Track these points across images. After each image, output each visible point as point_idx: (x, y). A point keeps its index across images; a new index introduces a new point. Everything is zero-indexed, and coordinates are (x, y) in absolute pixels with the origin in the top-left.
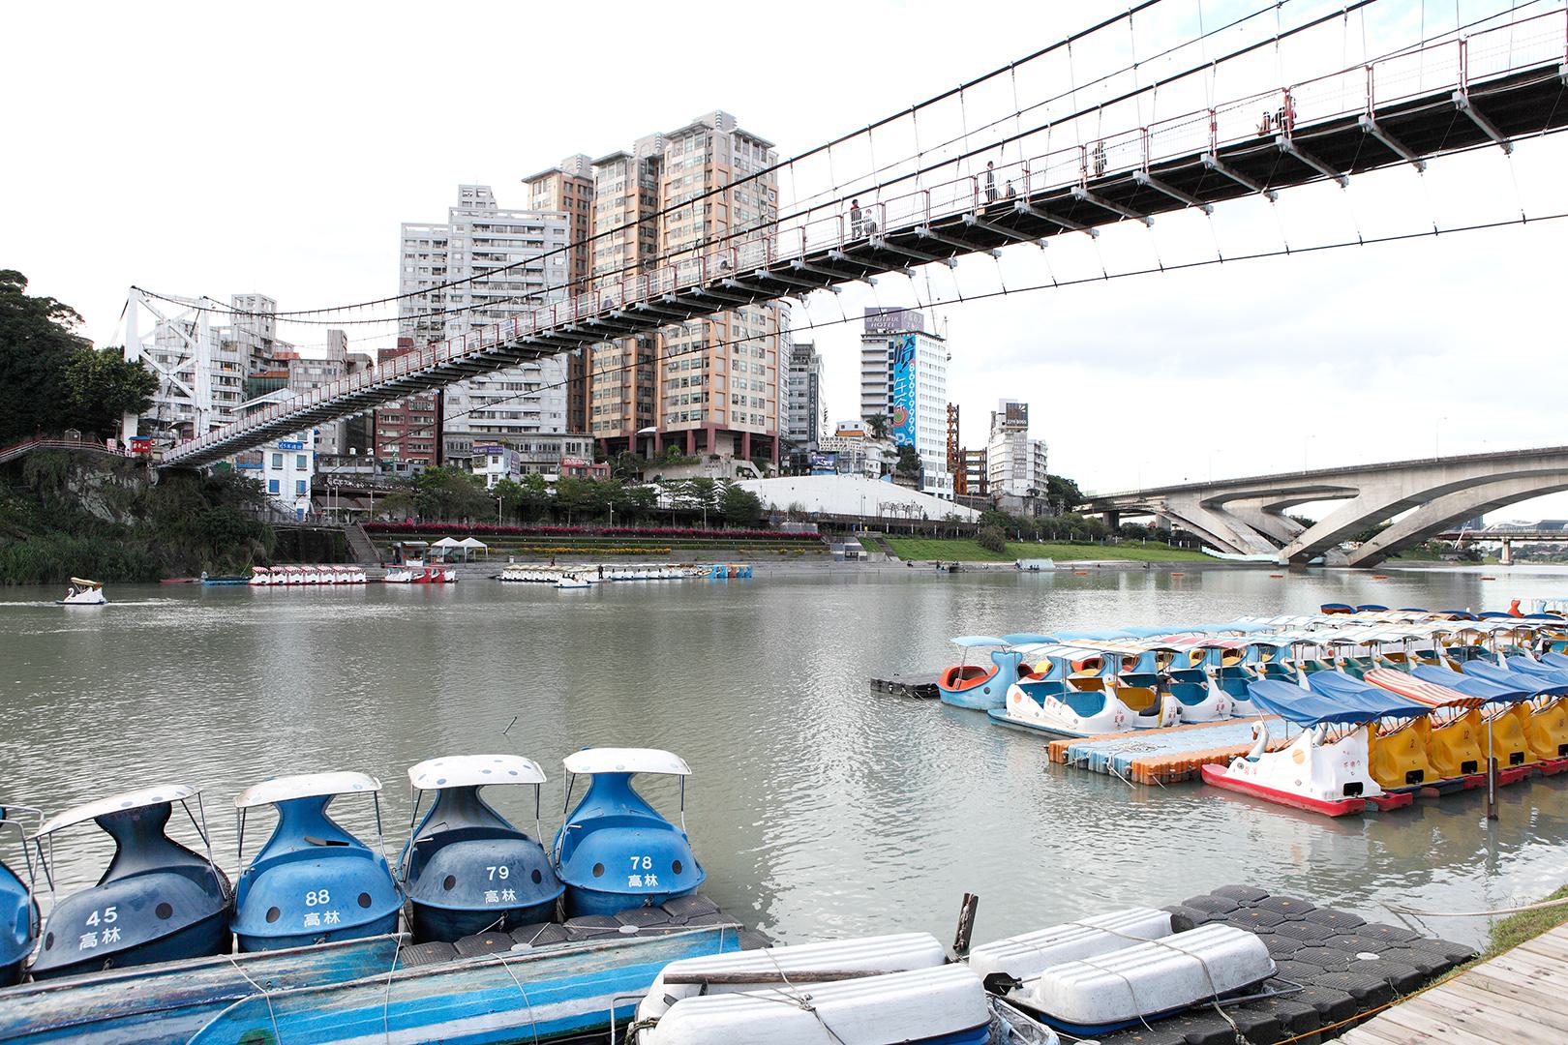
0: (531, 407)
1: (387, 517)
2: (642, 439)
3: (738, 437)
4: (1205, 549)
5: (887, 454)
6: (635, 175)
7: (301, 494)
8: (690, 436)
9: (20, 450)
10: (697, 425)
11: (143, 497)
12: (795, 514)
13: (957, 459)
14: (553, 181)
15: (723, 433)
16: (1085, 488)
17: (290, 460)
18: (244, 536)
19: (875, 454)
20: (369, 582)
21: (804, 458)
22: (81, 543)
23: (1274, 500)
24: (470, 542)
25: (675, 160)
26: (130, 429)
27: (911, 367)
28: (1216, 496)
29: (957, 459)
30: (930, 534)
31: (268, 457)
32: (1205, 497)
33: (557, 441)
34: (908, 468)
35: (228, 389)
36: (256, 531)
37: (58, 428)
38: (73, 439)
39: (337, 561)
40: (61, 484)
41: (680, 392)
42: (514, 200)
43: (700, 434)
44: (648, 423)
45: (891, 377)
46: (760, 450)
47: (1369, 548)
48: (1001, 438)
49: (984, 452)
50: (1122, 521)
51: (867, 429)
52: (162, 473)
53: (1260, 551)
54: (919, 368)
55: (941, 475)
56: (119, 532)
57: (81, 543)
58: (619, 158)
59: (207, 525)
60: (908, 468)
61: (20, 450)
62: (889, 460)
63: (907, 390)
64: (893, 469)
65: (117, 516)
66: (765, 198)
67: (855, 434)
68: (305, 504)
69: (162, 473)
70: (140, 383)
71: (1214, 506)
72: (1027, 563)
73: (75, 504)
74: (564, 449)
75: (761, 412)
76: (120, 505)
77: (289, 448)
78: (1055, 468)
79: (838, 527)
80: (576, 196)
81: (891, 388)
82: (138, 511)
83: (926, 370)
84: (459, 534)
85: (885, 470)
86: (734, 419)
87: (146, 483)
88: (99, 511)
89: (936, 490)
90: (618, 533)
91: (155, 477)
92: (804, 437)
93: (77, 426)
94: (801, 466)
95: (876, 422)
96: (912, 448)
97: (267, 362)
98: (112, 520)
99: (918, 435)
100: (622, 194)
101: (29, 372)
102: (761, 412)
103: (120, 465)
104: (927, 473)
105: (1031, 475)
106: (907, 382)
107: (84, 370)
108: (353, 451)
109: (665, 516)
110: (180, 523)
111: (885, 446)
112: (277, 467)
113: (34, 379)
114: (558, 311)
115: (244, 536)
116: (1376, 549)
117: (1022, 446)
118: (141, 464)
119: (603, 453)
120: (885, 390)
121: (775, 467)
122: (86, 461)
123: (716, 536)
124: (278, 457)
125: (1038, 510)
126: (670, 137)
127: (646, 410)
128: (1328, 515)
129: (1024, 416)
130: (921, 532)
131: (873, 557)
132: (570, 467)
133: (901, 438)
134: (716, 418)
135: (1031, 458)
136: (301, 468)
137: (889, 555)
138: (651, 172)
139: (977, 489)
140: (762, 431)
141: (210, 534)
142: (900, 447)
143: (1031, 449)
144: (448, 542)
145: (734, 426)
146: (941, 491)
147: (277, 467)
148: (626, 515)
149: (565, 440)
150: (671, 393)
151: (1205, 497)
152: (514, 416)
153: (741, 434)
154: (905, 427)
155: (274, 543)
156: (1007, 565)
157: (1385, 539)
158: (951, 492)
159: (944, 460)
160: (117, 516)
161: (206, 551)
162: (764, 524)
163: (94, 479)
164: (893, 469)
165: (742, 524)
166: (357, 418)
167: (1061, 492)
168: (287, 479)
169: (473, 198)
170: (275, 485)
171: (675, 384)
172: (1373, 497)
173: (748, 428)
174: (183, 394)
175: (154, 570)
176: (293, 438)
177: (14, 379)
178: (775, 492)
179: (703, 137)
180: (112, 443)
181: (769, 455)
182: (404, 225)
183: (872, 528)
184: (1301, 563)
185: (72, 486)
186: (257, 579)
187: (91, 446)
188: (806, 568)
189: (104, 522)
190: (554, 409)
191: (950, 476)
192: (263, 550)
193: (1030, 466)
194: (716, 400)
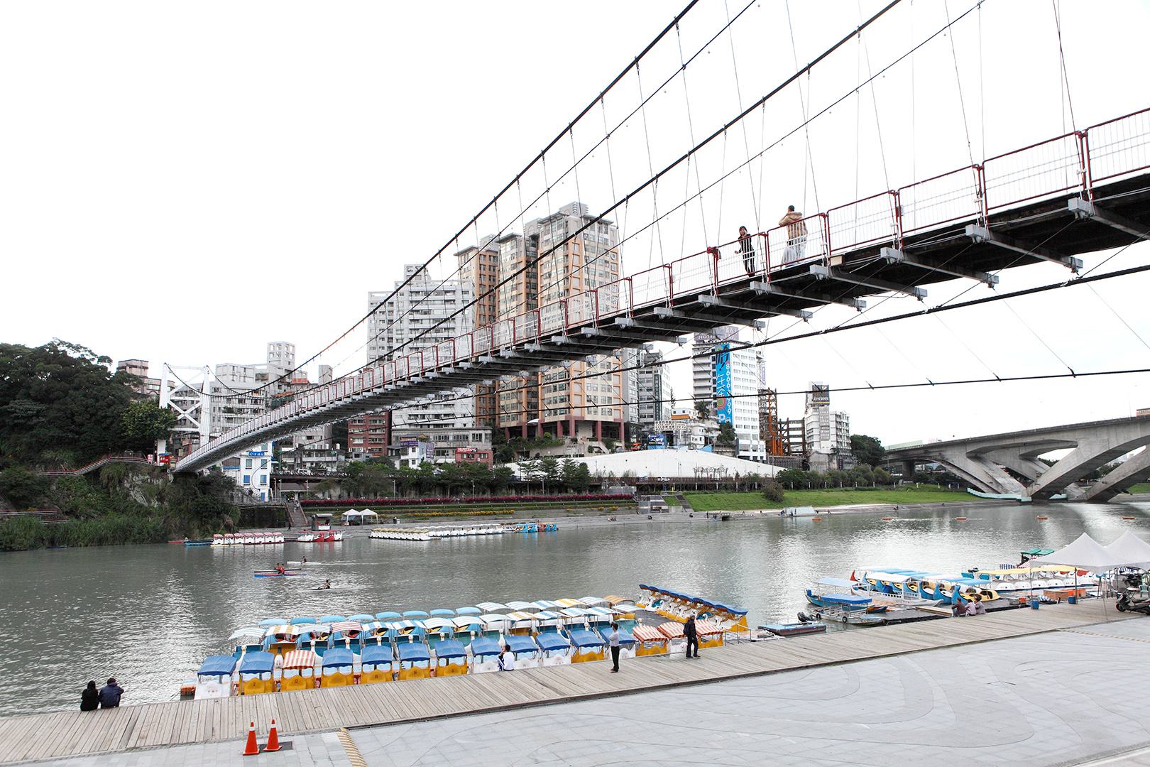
0: (448, 411)
1: (320, 496)
2: (532, 428)
3: (594, 424)
4: (969, 490)
5: (708, 430)
6: (523, 248)
7: (263, 483)
8: (559, 425)
9: (100, 463)
10: (562, 418)
11: (164, 490)
12: (627, 480)
13: (770, 426)
14: (471, 254)
15: (581, 423)
16: (887, 443)
17: (257, 463)
18: (219, 513)
19: (698, 431)
20: (286, 541)
21: (646, 436)
22: (121, 520)
24: (367, 512)
25: (546, 238)
26: (161, 449)
27: (727, 366)
28: (980, 448)
29: (770, 426)
30: (733, 489)
31: (243, 462)
32: (971, 448)
34: (726, 440)
35: (255, 407)
36: (227, 509)
37: (120, 449)
38: (129, 457)
39: (280, 526)
40: (120, 482)
42: (444, 271)
43: (565, 424)
44: (536, 416)
45: (714, 374)
46: (611, 434)
48: (811, 410)
49: (803, 421)
50: (918, 467)
51: (694, 414)
52: (175, 475)
53: (1016, 490)
54: (733, 367)
55: (755, 442)
56: (149, 513)
57: (121, 520)
58: (512, 237)
59: (205, 502)
60: (726, 440)
61: (100, 463)
62: (710, 435)
63: (725, 383)
64: (715, 440)
65: (149, 502)
67: (684, 417)
68: (266, 490)
69: (175, 475)
70: (165, 422)
71: (976, 456)
72: (789, 511)
73: (128, 495)
74: (470, 438)
76: (151, 495)
77: (255, 455)
78: (857, 429)
79: (651, 487)
80: (488, 263)
81: (714, 382)
82: (161, 499)
83: (739, 367)
84: (360, 505)
85: (708, 441)
87: (167, 481)
88: (140, 499)
89: (751, 454)
90: (478, 501)
91: (171, 478)
92: (651, 420)
93: (131, 448)
94: (645, 443)
95: (701, 408)
96: (729, 425)
97: (289, 385)
98: (146, 504)
99: (734, 415)
100: (515, 261)
101: (106, 417)
103: (153, 471)
104: (741, 442)
105: (834, 438)
106: (725, 377)
107: (132, 416)
108: (338, 446)
109: (520, 486)
110: (182, 507)
111: (708, 424)
112: (249, 467)
113: (108, 421)
114: (464, 346)
115: (219, 513)
116: (1104, 487)
117: (826, 416)
118: (164, 470)
119: (491, 439)
120: (710, 384)
121: (622, 444)
122: (134, 468)
123: (551, 500)
124: (249, 461)
125: (841, 463)
126: (542, 223)
127: (533, 410)
128: (1063, 459)
130: (726, 487)
131: (673, 509)
132: (462, 453)
133: (722, 418)
134: (576, 413)
135: (833, 425)
136: (264, 466)
137: (685, 507)
138: (533, 245)
139: (800, 448)
140: (611, 419)
141: (198, 513)
142: (722, 424)
143: (833, 418)
144: (352, 512)
145: (588, 418)
146: (755, 454)
147: (249, 467)
148: (493, 486)
150: (547, 396)
151: (971, 448)
152: (437, 416)
153: (595, 422)
154: (726, 410)
155: (238, 517)
156: (773, 512)
157: (1113, 478)
158: (764, 454)
159: (757, 431)
160: (149, 502)
161: (196, 523)
162: (596, 488)
163: (138, 479)
164: (715, 440)
165: (580, 490)
166: (339, 421)
167: (865, 449)
168: (253, 475)
170: (247, 479)
172: (1089, 450)
173: (600, 418)
174: (195, 427)
175: (165, 535)
176: (258, 449)
177: (98, 422)
178: (607, 464)
179: (562, 221)
180: (150, 457)
181: (617, 437)
182: (371, 294)
183: (678, 488)
184: (1042, 498)
185: (127, 485)
186: (216, 542)
187: (138, 460)
188: (623, 518)
189: (141, 506)
191: (763, 443)
192: (230, 520)
193: (833, 431)
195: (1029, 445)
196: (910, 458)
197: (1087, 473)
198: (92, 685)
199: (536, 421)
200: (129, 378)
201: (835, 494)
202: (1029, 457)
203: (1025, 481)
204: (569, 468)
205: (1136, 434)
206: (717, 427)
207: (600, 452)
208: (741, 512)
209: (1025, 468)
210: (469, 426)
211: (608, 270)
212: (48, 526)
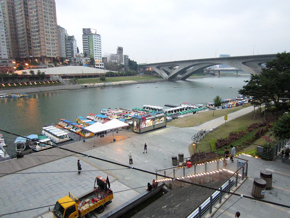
23: (170, 66)
28: (159, 66)
33: (6, 60)
34: (92, 63)
41: (34, 30)
46: (56, 61)
47: (184, 75)
60: (92, 63)
66: (52, 5)
74: (8, 62)
75: (55, 53)
86: (48, 54)
92: (70, 56)
94: (69, 63)
96: (93, 58)
102: (55, 53)
111: (87, 58)
128: (178, 68)
129: (122, 50)
134: (44, 55)
143: (123, 57)
146: (101, 67)
149: (8, 60)
151: (169, 67)
157: (187, 74)
169: (106, 134)
171: (33, 28)
173: (52, 56)
190: (5, 53)
194: (43, 51)
195: (171, 65)
196: (144, 67)
197: (182, 72)
198: (149, 184)
199: (32, 56)
200: (136, 62)
201: (122, 77)
202: (171, 68)
203: (168, 73)
204: (39, 73)
205: (191, 64)
206: (89, 59)
207: (53, 67)
208: (92, 84)
209: (169, 71)
210: (7, 58)
211: (52, 9)
212: (107, 120)
